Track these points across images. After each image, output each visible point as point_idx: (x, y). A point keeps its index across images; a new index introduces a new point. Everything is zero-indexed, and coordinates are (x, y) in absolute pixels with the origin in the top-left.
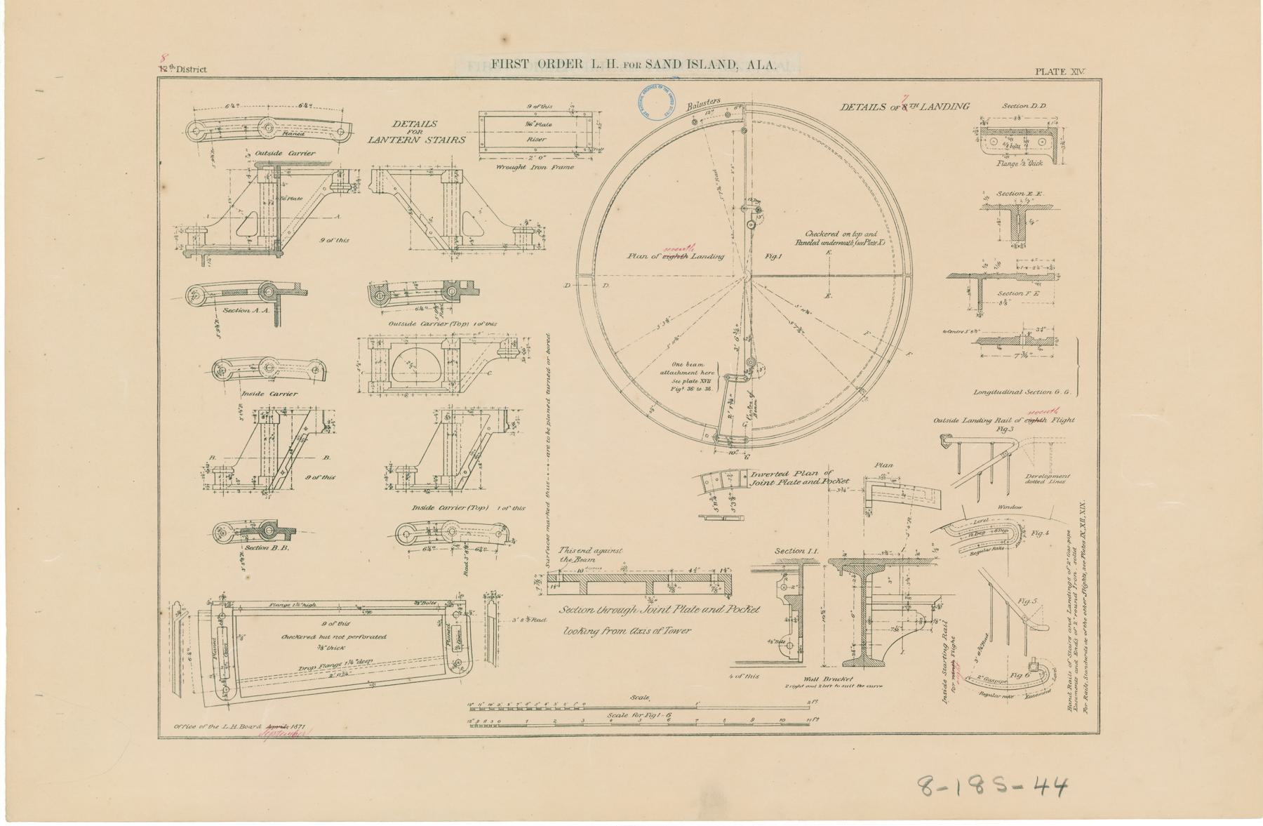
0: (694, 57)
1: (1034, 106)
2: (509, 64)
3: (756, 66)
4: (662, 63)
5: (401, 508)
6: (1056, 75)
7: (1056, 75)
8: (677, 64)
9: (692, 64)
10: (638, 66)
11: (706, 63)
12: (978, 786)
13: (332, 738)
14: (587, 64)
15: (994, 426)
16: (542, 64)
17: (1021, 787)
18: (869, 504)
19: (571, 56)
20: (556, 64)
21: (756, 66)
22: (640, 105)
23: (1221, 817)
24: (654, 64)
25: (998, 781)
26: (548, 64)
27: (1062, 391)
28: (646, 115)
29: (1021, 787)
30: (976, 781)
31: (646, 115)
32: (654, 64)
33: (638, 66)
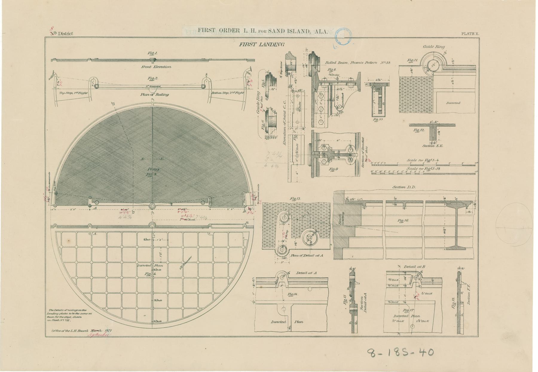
2: (206, 30)
3: (318, 32)
4: (276, 30)
8: (283, 31)
9: (290, 31)
10: (265, 32)
11: (296, 31)
12: (372, 353)
14: (242, 31)
20: (227, 31)
21: (318, 32)
24: (272, 31)
25: (404, 350)
26: (224, 30)
30: (371, 351)
32: (272, 31)
33: (265, 32)
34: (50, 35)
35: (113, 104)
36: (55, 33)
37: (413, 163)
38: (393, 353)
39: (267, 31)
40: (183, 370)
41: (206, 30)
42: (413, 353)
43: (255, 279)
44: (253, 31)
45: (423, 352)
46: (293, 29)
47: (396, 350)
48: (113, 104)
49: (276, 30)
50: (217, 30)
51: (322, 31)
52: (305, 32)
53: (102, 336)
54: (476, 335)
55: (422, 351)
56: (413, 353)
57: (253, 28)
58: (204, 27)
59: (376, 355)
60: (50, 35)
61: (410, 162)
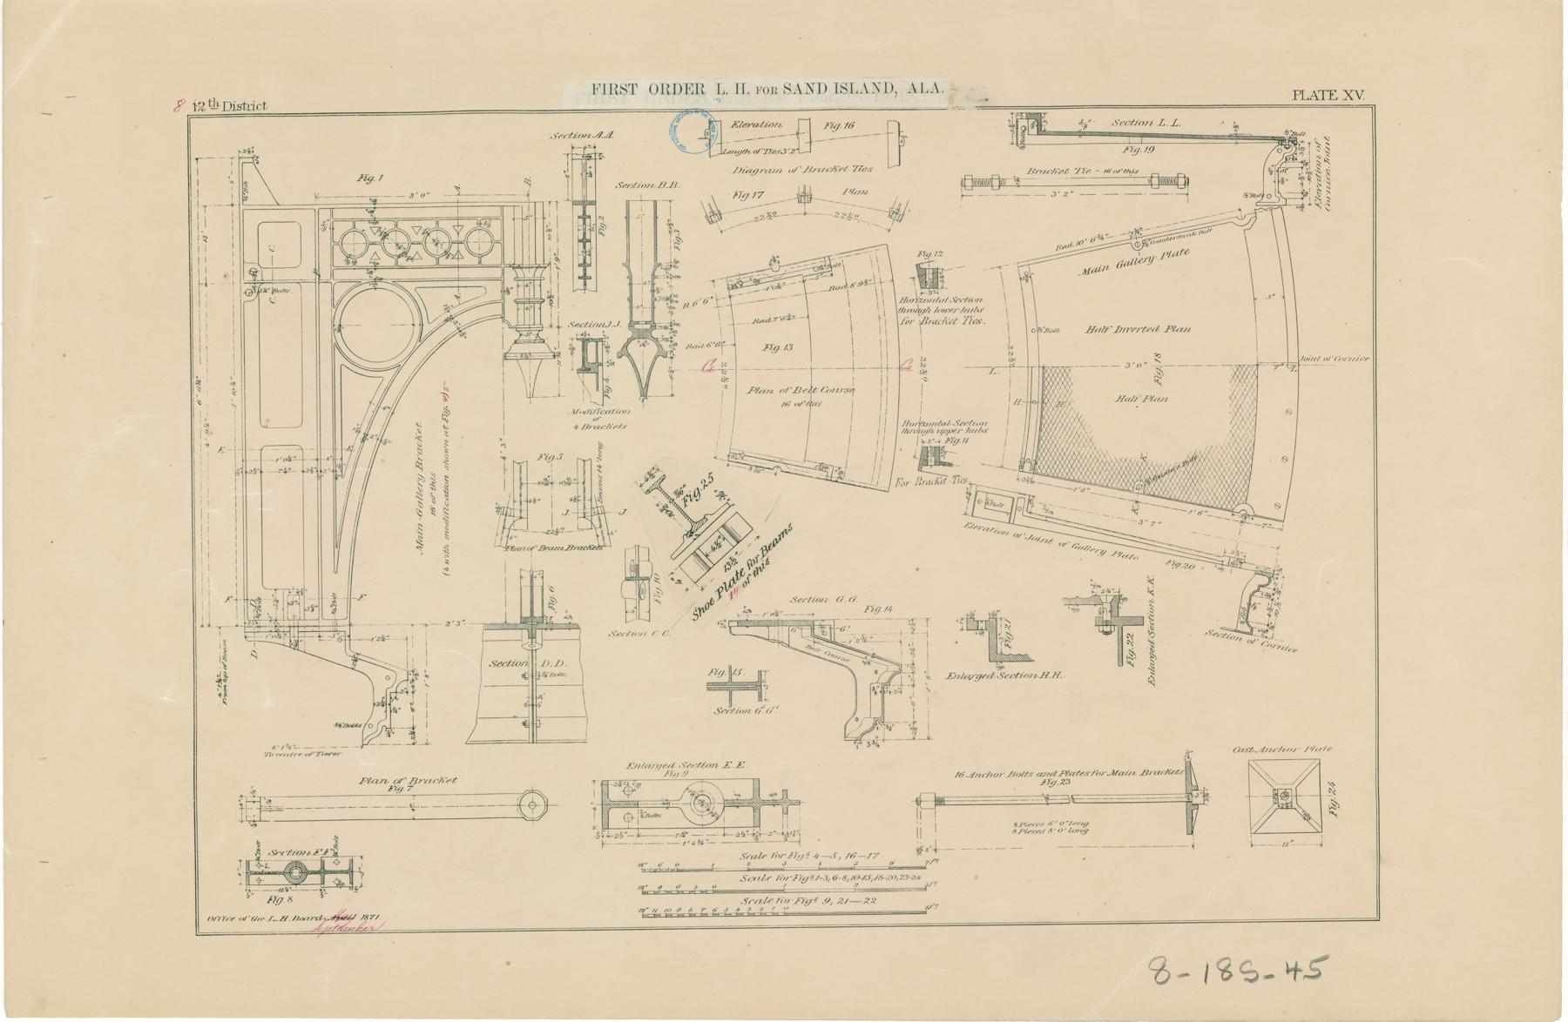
1: (663, 185)
2: (614, 90)
3: (918, 88)
4: (804, 88)
5: (247, 794)
6: (1324, 97)
7: (1324, 97)
9: (841, 89)
10: (773, 91)
11: (858, 87)
14: (710, 89)
15: (441, 472)
18: (1056, 826)
20: (671, 89)
21: (918, 88)
22: (674, 139)
24: (794, 88)
25: (1245, 968)
26: (663, 89)
28: (682, 147)
31: (682, 147)
32: (794, 88)
33: (773, 91)
35: (254, 654)
37: (756, 864)
38: (1215, 974)
39: (781, 89)
41: (614, 90)
43: (1022, 475)
44: (740, 89)
46: (848, 81)
47: (1222, 966)
48: (254, 654)
49: (804, 88)
50: (642, 89)
51: (929, 86)
54: (1374, 916)
55: (1292, 966)
57: (740, 82)
58: (608, 82)
61: (745, 861)
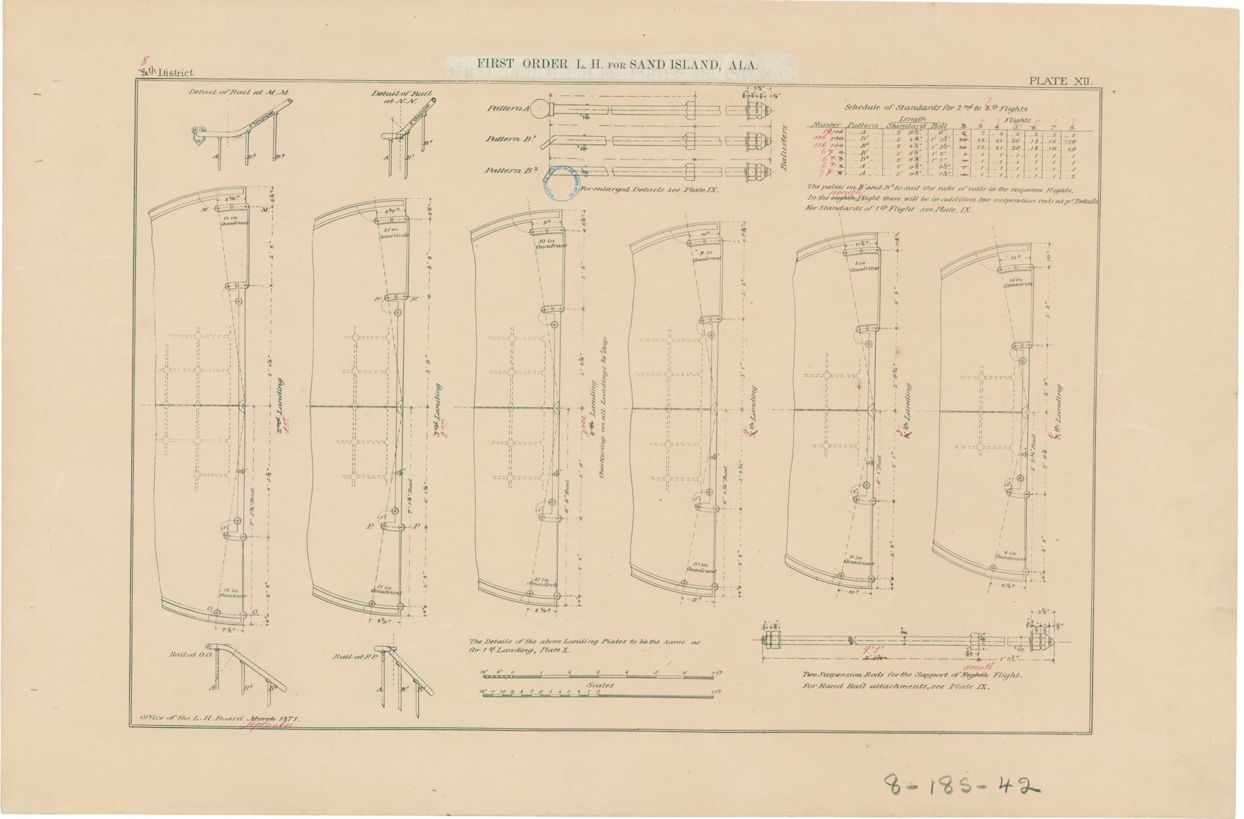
0: (676, 58)
2: (495, 64)
3: (738, 66)
4: (646, 64)
7: (1057, 83)
8: (661, 64)
9: (676, 65)
10: (622, 66)
11: (689, 64)
12: (948, 785)
13: (833, 732)
14: (572, 63)
16: (761, 142)
17: (915, 787)
19: (559, 56)
20: (541, 64)
21: (738, 66)
23: (123, 813)
24: (638, 64)
26: (534, 64)
27: (273, 252)
29: (915, 787)
30: (946, 781)
32: (638, 64)
33: (622, 66)
34: (140, 75)
36: (152, 70)
38: (939, 788)
39: (628, 64)
40: (892, 816)
42: (983, 787)
45: (1007, 786)
52: (656, 64)
53: (275, 728)
55: (1005, 783)
56: (983, 787)
58: (490, 57)
59: (904, 790)
60: (140, 75)
